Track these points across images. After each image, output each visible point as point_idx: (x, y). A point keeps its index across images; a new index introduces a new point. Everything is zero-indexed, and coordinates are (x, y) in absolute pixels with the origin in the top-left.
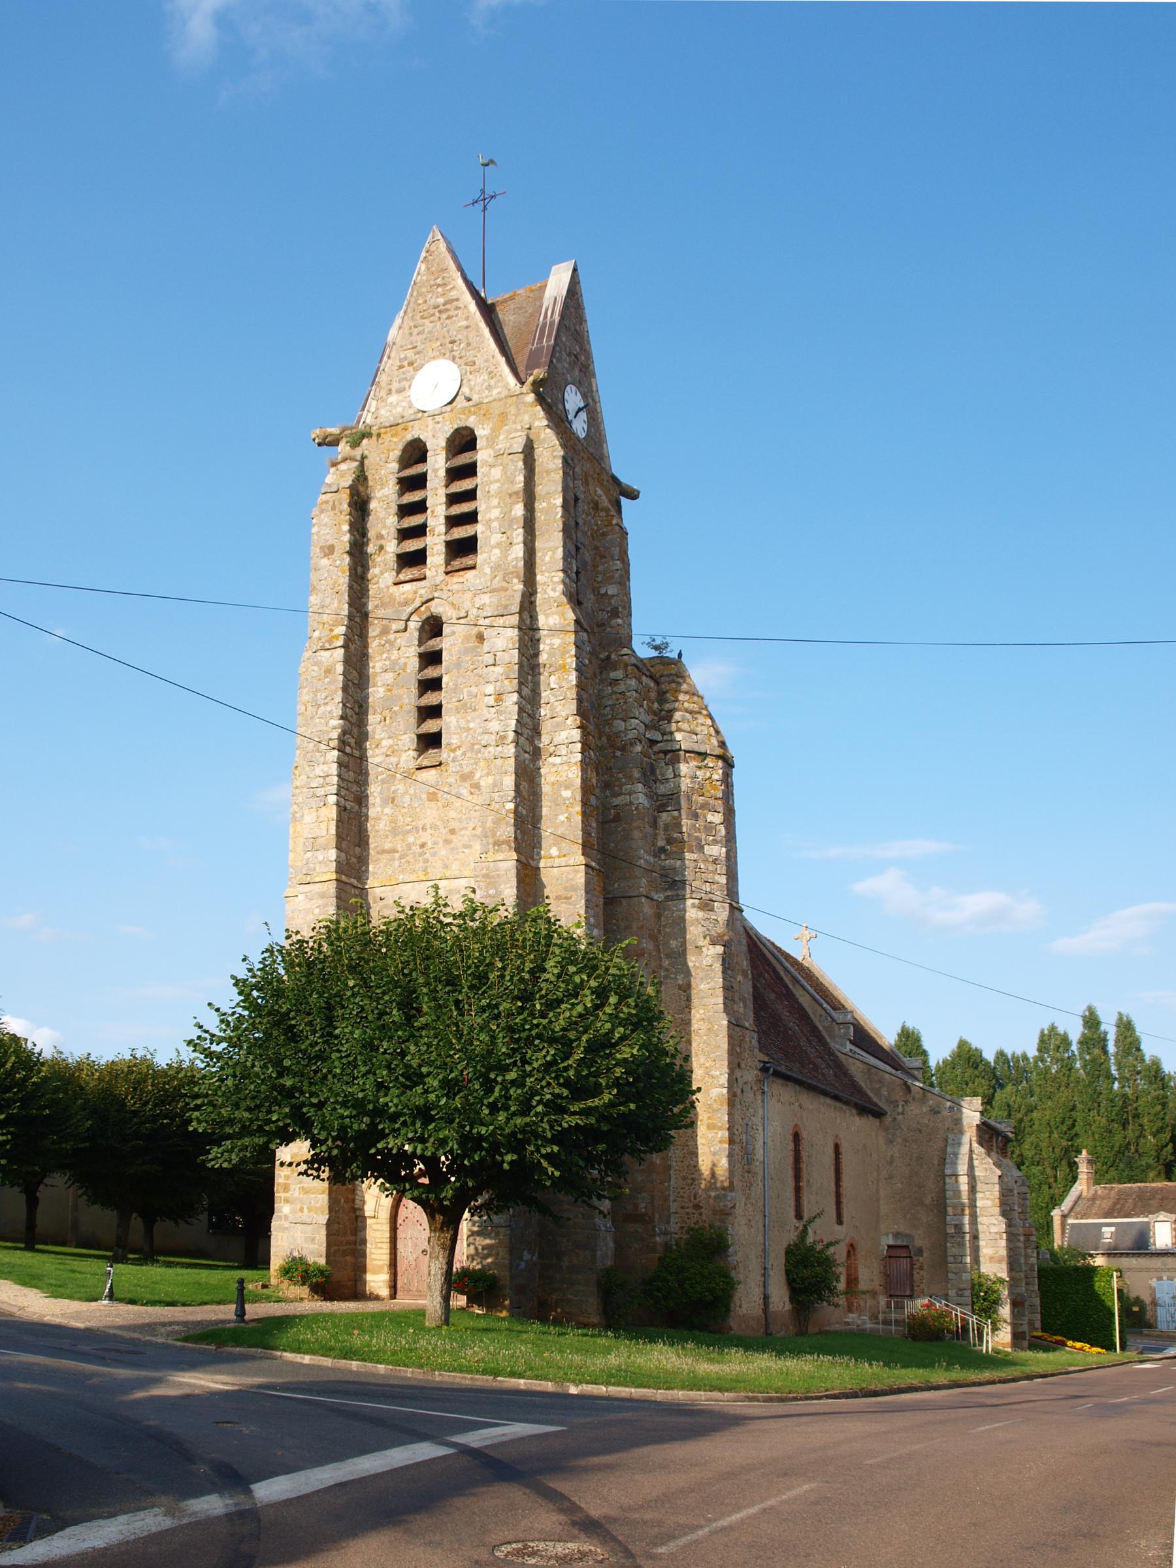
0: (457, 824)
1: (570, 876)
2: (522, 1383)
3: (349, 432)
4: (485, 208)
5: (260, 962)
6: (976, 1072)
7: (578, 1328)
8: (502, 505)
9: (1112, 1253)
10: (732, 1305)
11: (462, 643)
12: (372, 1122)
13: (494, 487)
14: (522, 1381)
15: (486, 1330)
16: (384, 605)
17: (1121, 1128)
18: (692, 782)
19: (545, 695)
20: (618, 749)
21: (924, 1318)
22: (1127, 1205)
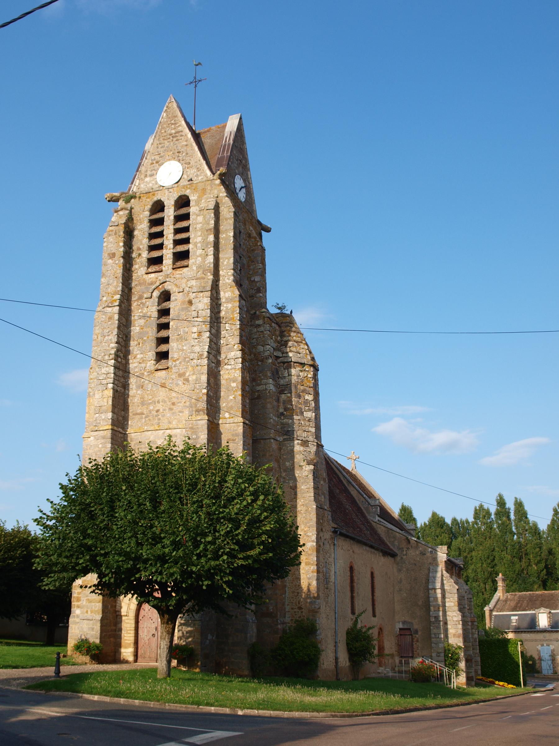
0: (176, 400)
1: (235, 429)
2: (213, 709)
3: (125, 195)
4: (196, 86)
5: (75, 476)
6: (442, 530)
7: (238, 678)
8: (203, 235)
9: (517, 630)
10: (319, 663)
11: (181, 305)
12: (134, 564)
13: (199, 226)
14: (213, 708)
15: (189, 680)
16: (140, 284)
17: (519, 561)
18: (297, 379)
19: (223, 333)
20: (260, 361)
21: (420, 669)
22: (524, 604)
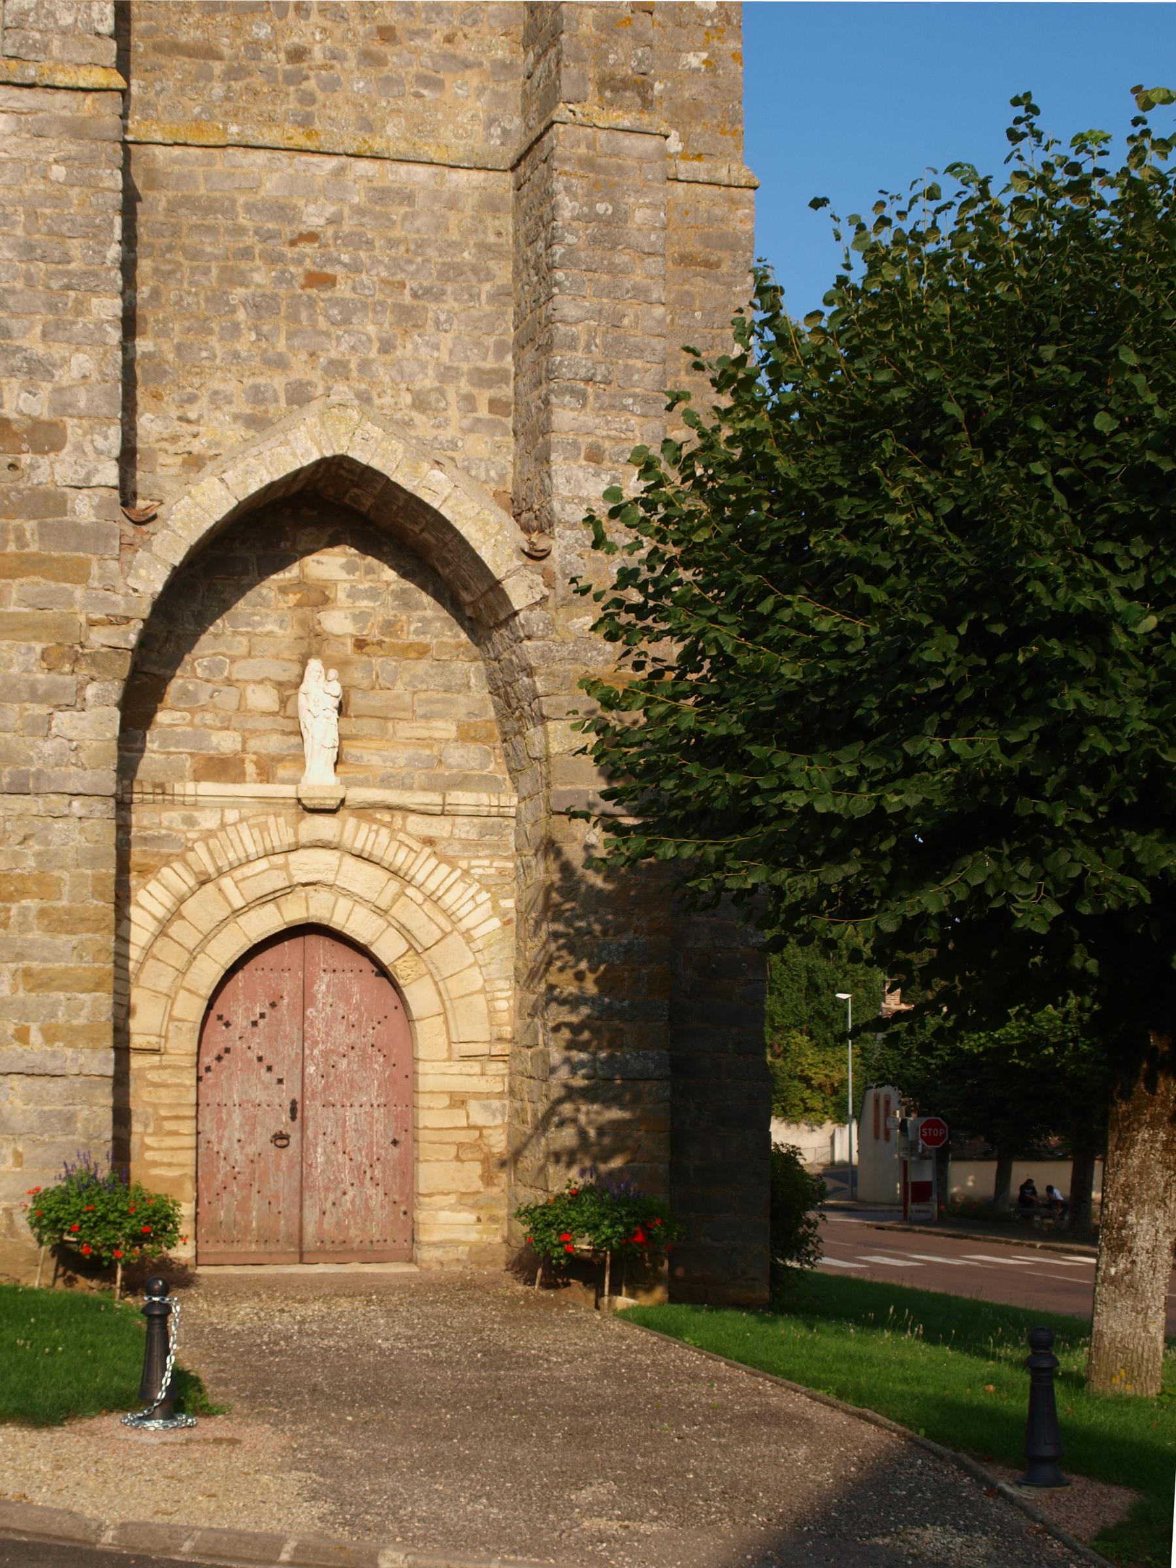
1: (717, 211)
